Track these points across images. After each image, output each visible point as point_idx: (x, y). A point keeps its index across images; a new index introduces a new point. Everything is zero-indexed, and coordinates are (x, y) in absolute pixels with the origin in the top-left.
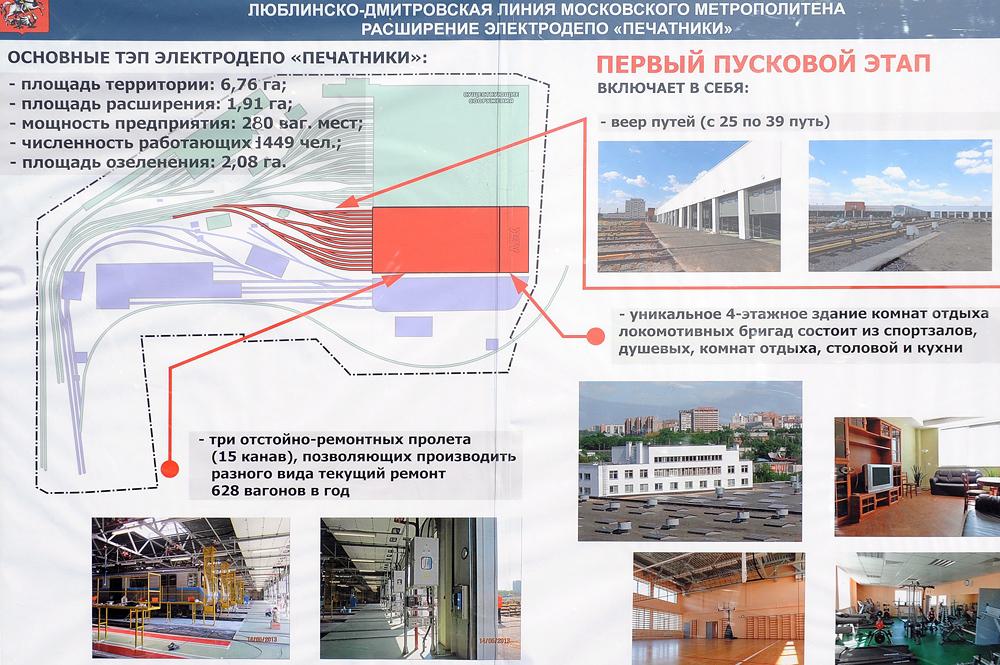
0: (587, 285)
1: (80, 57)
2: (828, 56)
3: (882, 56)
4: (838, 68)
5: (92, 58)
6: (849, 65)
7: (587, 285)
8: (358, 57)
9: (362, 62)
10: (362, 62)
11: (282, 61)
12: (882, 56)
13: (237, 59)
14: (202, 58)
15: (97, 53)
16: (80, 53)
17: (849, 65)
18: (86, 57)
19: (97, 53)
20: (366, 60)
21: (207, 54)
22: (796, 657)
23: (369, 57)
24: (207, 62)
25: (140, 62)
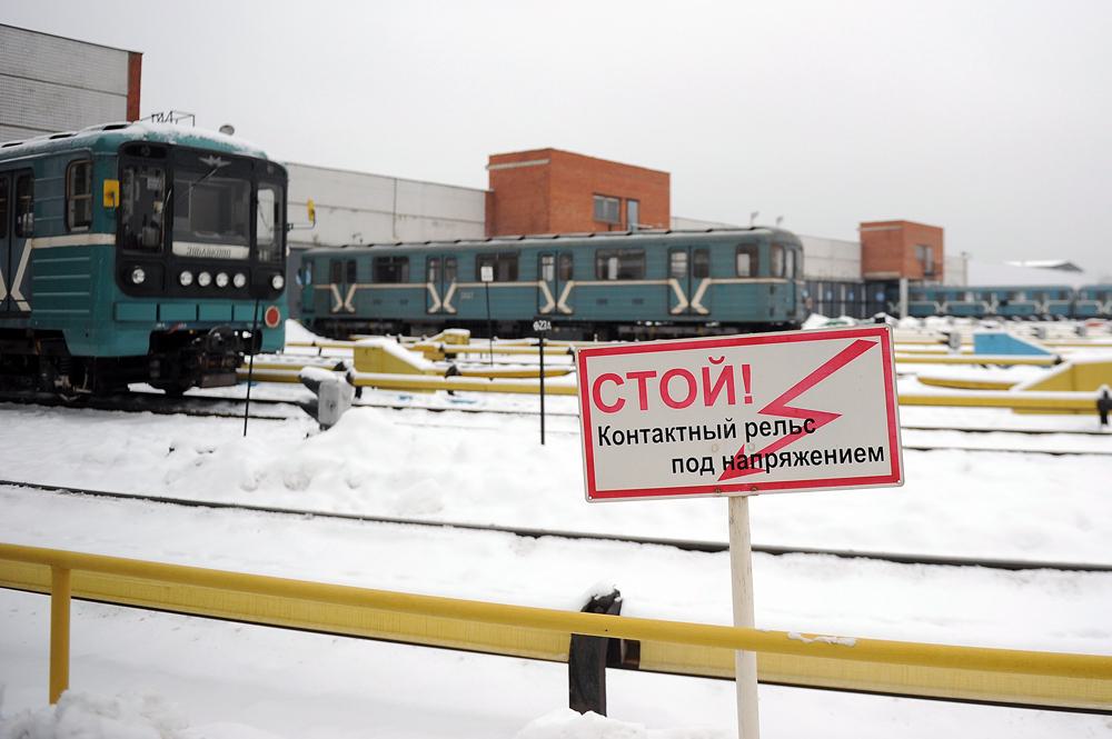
0: (589, 360)
1: (698, 433)
2: (677, 405)
3: (630, 376)
4: (779, 464)
5: (713, 433)
6: (713, 383)
7: (589, 360)
8: (686, 432)
9: (691, 439)
10: (691, 439)
11: (615, 433)
12: (630, 376)
13: (700, 467)
14: (676, 434)
15: (719, 426)
16: (834, 451)
17: (713, 383)
18: (706, 432)
19: (719, 426)
20: (695, 436)
21: (681, 429)
22: (125, 99)
23: (834, 456)
24: (682, 439)
25: (720, 437)
